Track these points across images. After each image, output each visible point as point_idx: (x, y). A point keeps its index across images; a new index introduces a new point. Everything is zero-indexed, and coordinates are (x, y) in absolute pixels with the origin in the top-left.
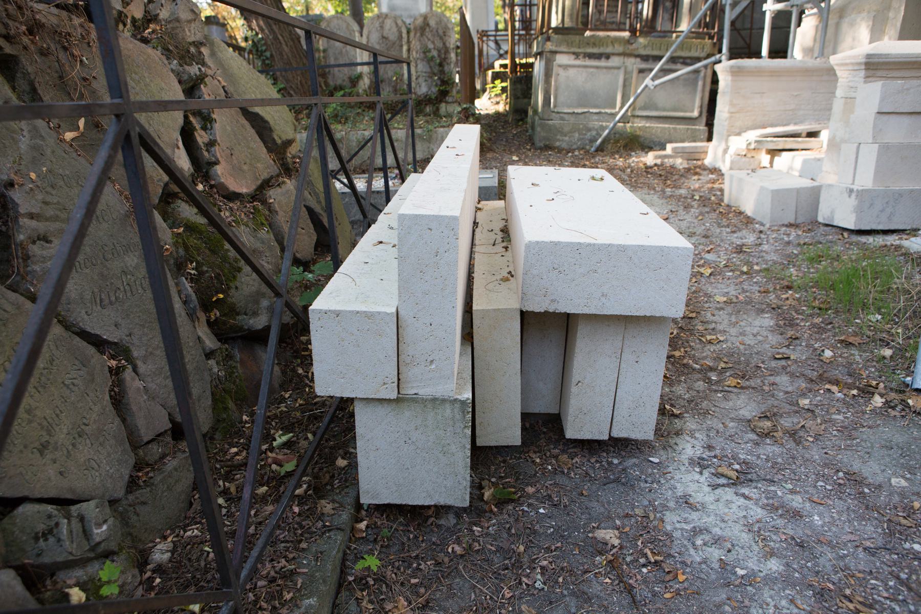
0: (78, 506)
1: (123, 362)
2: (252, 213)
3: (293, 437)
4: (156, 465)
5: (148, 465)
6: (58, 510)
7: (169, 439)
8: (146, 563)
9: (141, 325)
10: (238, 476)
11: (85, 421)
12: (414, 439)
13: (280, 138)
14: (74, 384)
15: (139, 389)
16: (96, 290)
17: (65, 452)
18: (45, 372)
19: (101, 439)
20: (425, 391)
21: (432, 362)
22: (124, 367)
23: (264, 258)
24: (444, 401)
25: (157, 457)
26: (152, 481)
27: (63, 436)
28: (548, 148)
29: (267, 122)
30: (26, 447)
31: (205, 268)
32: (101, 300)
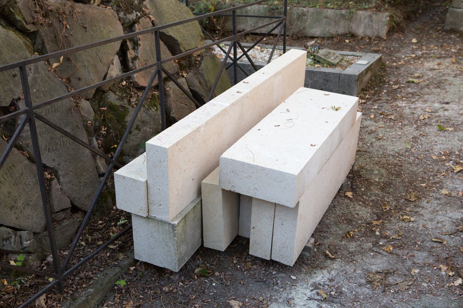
0: (20, 232)
1: (53, 176)
2: (150, 99)
3: (127, 222)
4: (59, 222)
5: (56, 221)
6: (12, 231)
7: (69, 212)
8: (45, 260)
9: (65, 161)
10: (95, 234)
11: (30, 199)
12: (155, 236)
13: (185, 49)
14: (29, 184)
15: (58, 189)
16: (48, 144)
17: (20, 211)
18: (18, 178)
19: (36, 208)
20: (159, 217)
21: (160, 205)
22: (53, 179)
23: (149, 126)
24: (165, 223)
25: (61, 219)
26: (55, 228)
27: (20, 204)
28: (453, 31)
29: (176, 40)
30: (5, 206)
31: (111, 131)
32: (49, 149)
